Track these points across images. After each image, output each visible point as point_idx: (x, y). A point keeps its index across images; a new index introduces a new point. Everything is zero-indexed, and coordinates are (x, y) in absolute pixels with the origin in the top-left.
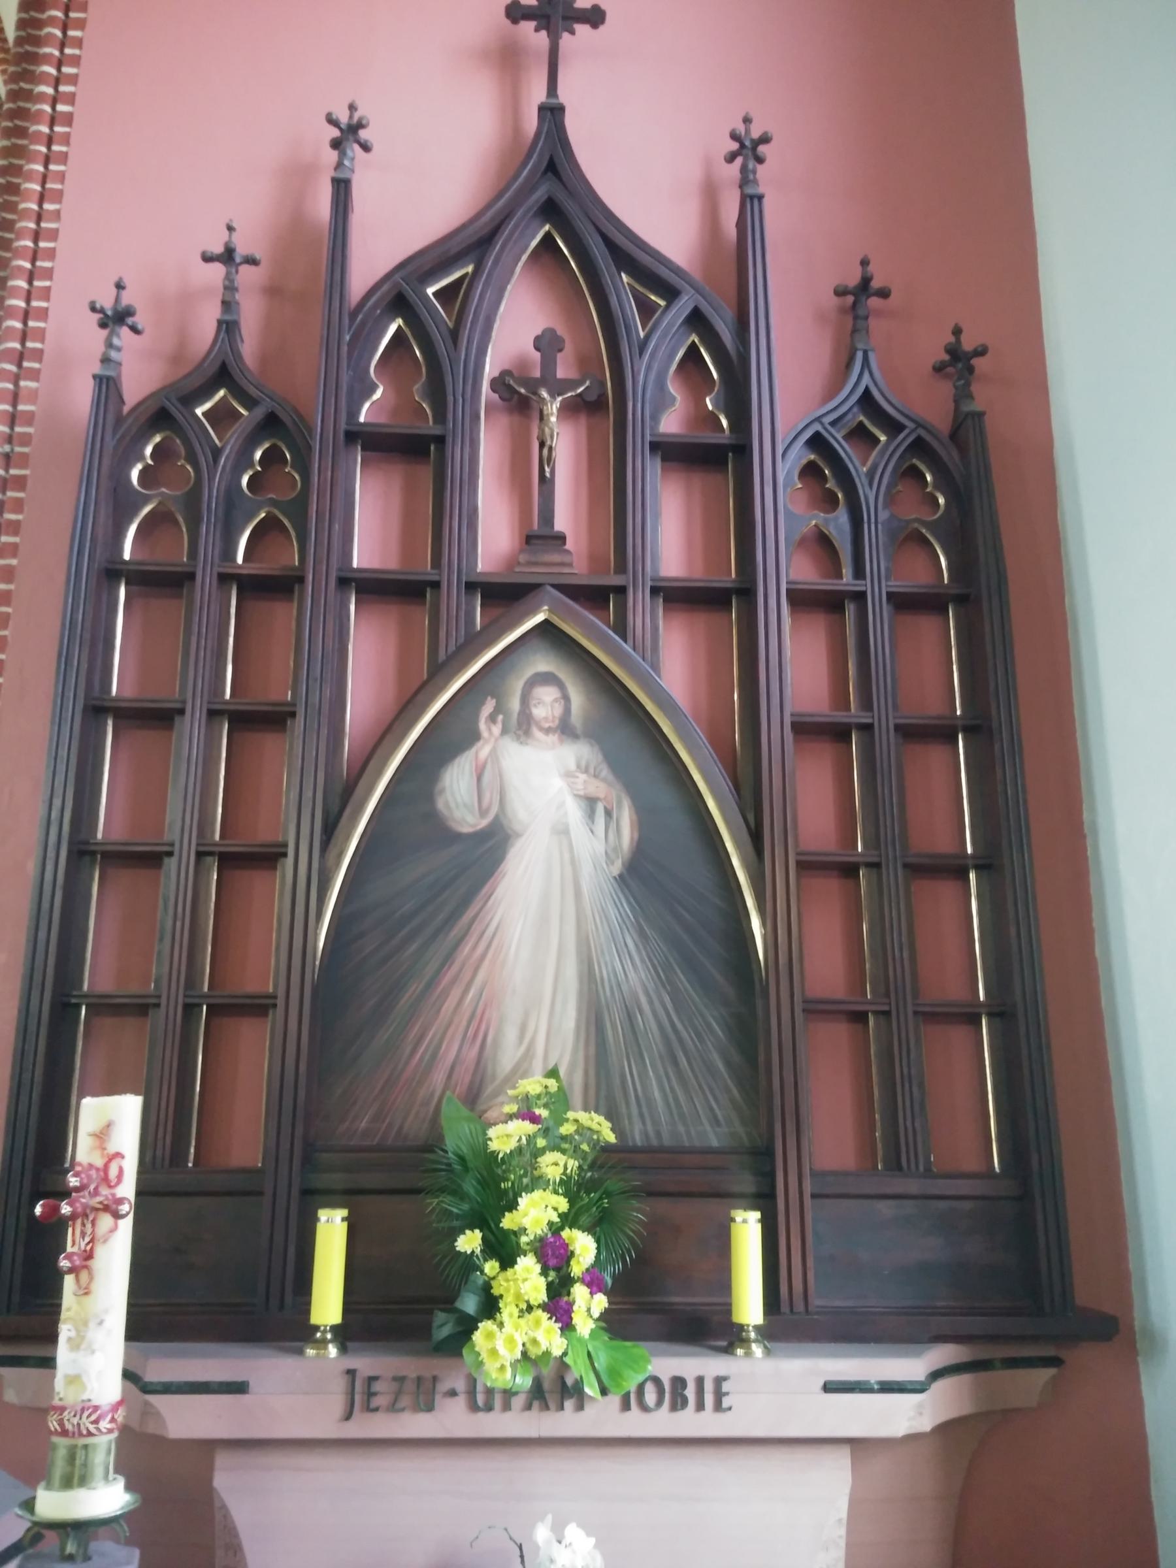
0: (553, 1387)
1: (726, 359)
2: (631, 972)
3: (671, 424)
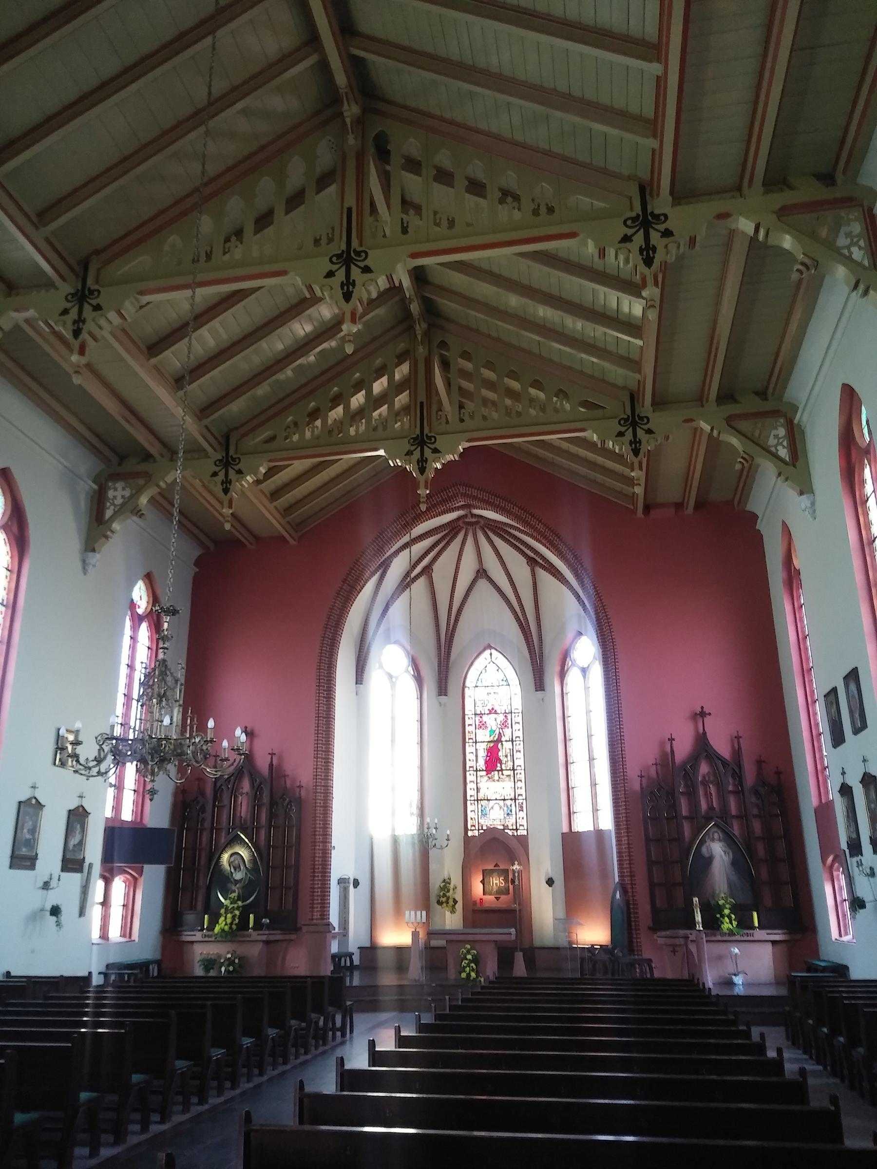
0: (731, 933)
1: (738, 775)
2: (734, 878)
3: (731, 788)
